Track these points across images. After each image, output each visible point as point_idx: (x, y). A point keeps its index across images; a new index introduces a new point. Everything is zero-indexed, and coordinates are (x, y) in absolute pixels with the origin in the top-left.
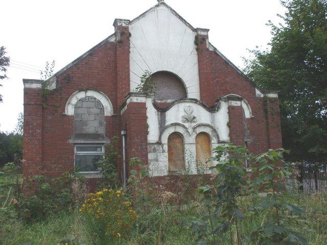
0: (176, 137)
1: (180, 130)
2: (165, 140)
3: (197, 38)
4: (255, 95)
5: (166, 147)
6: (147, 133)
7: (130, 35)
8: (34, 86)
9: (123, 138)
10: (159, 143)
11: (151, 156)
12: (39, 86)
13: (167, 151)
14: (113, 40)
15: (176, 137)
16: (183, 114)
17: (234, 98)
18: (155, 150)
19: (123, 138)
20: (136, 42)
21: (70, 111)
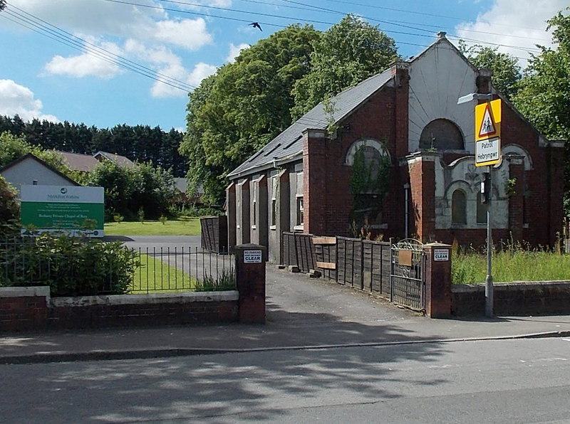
0: (460, 195)
1: (464, 187)
2: (450, 196)
3: (478, 79)
4: (538, 144)
5: (450, 203)
6: (435, 189)
7: (409, 78)
8: (318, 135)
9: (406, 191)
10: (445, 198)
11: (437, 211)
12: (322, 135)
13: (451, 205)
14: (391, 84)
15: (460, 195)
16: (466, 172)
17: (294, 372)
18: (440, 206)
19: (406, 191)
20: (415, 85)
21: (350, 160)
